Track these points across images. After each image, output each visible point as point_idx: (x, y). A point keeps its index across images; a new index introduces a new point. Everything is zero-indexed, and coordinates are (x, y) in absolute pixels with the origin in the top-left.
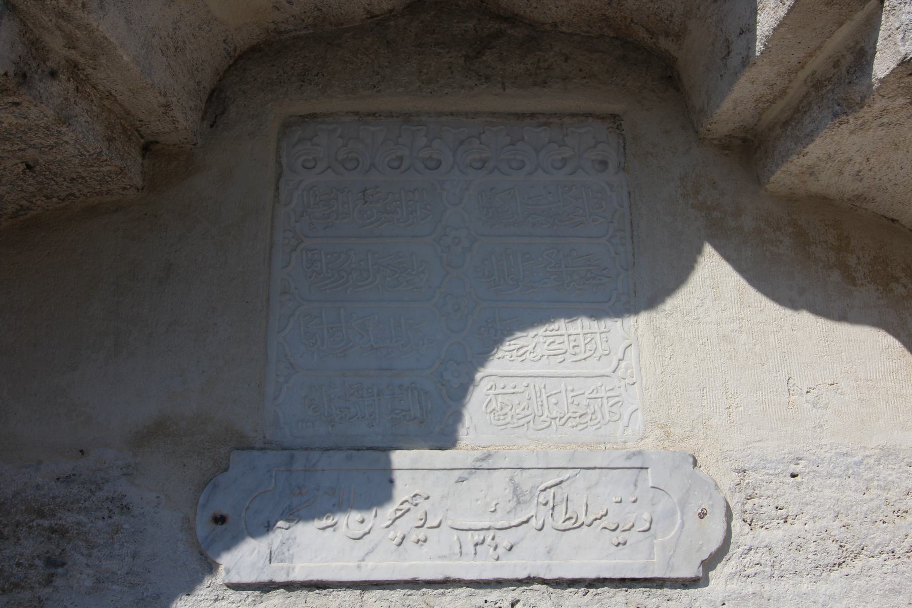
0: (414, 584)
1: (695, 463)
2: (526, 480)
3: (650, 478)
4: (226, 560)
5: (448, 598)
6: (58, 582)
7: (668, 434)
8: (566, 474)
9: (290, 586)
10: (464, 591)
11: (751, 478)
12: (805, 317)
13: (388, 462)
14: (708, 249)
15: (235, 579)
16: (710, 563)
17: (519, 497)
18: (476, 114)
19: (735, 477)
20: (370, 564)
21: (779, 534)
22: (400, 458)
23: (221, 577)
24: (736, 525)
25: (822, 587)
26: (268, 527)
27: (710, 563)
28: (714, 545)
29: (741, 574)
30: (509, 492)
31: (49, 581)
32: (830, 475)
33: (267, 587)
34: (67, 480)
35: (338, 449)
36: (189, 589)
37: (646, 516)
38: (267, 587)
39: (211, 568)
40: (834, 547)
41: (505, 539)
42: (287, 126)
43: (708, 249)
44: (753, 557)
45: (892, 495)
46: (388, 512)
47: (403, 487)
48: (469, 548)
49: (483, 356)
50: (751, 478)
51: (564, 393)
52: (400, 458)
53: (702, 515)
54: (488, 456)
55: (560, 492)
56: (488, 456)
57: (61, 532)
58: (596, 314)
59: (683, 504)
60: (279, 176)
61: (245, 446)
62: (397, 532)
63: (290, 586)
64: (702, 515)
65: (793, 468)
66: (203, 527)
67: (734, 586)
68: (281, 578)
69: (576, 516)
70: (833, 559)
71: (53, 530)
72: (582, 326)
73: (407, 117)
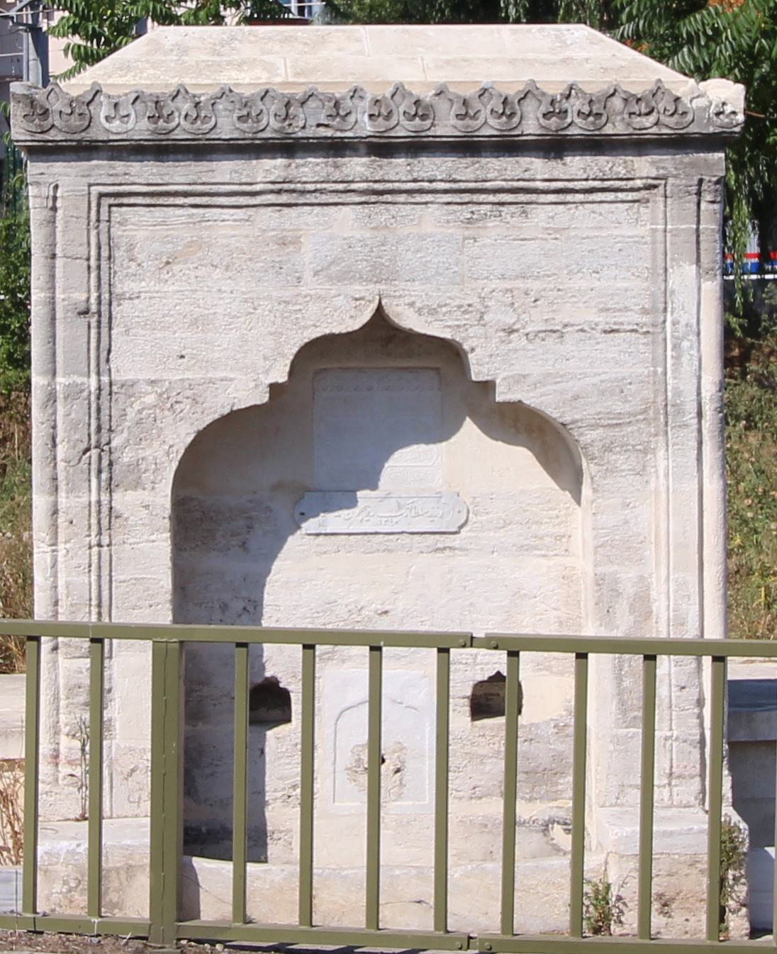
0: (366, 534)
1: (458, 495)
2: (402, 501)
3: (443, 500)
4: (304, 525)
5: (321, 621)
6: (252, 533)
7: (450, 486)
8: (415, 499)
9: (326, 534)
10: (381, 536)
11: (477, 500)
12: (500, 443)
13: (356, 495)
14: (468, 419)
15: (309, 532)
16: (461, 527)
17: (400, 507)
18: (385, 368)
19: (472, 499)
20: (351, 527)
21: (485, 518)
22: (359, 494)
23: (303, 531)
24: (471, 515)
25: (497, 535)
26: (317, 515)
27: (461, 527)
28: (463, 521)
29: (470, 531)
30: (396, 505)
31: (249, 532)
32: (503, 499)
33: (318, 535)
34: (251, 501)
35: (339, 491)
36: (292, 533)
37: (441, 512)
38: (318, 535)
39: (299, 528)
40: (502, 522)
41: (395, 520)
42: (316, 373)
43: (468, 419)
44: (476, 525)
45: (523, 505)
46: (356, 510)
47: (361, 504)
48: (383, 523)
49: (387, 458)
50: (477, 500)
51: (400, 500)
52: (359, 494)
53: (459, 512)
54: (389, 494)
55: (413, 505)
56: (389, 494)
57: (250, 518)
58: (427, 443)
59: (453, 509)
60: (314, 394)
61: (309, 491)
62: (360, 518)
63: (326, 534)
64: (459, 512)
65: (491, 497)
66: (297, 516)
67: (469, 534)
68: (323, 532)
69: (466, 509)
70: (501, 525)
71: (248, 517)
72: (423, 446)
73: (360, 370)
